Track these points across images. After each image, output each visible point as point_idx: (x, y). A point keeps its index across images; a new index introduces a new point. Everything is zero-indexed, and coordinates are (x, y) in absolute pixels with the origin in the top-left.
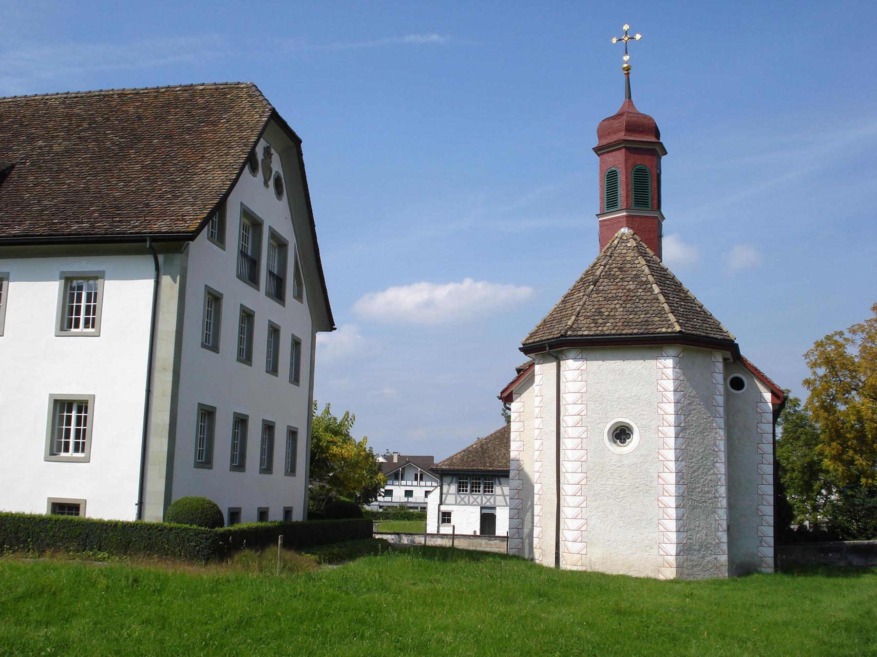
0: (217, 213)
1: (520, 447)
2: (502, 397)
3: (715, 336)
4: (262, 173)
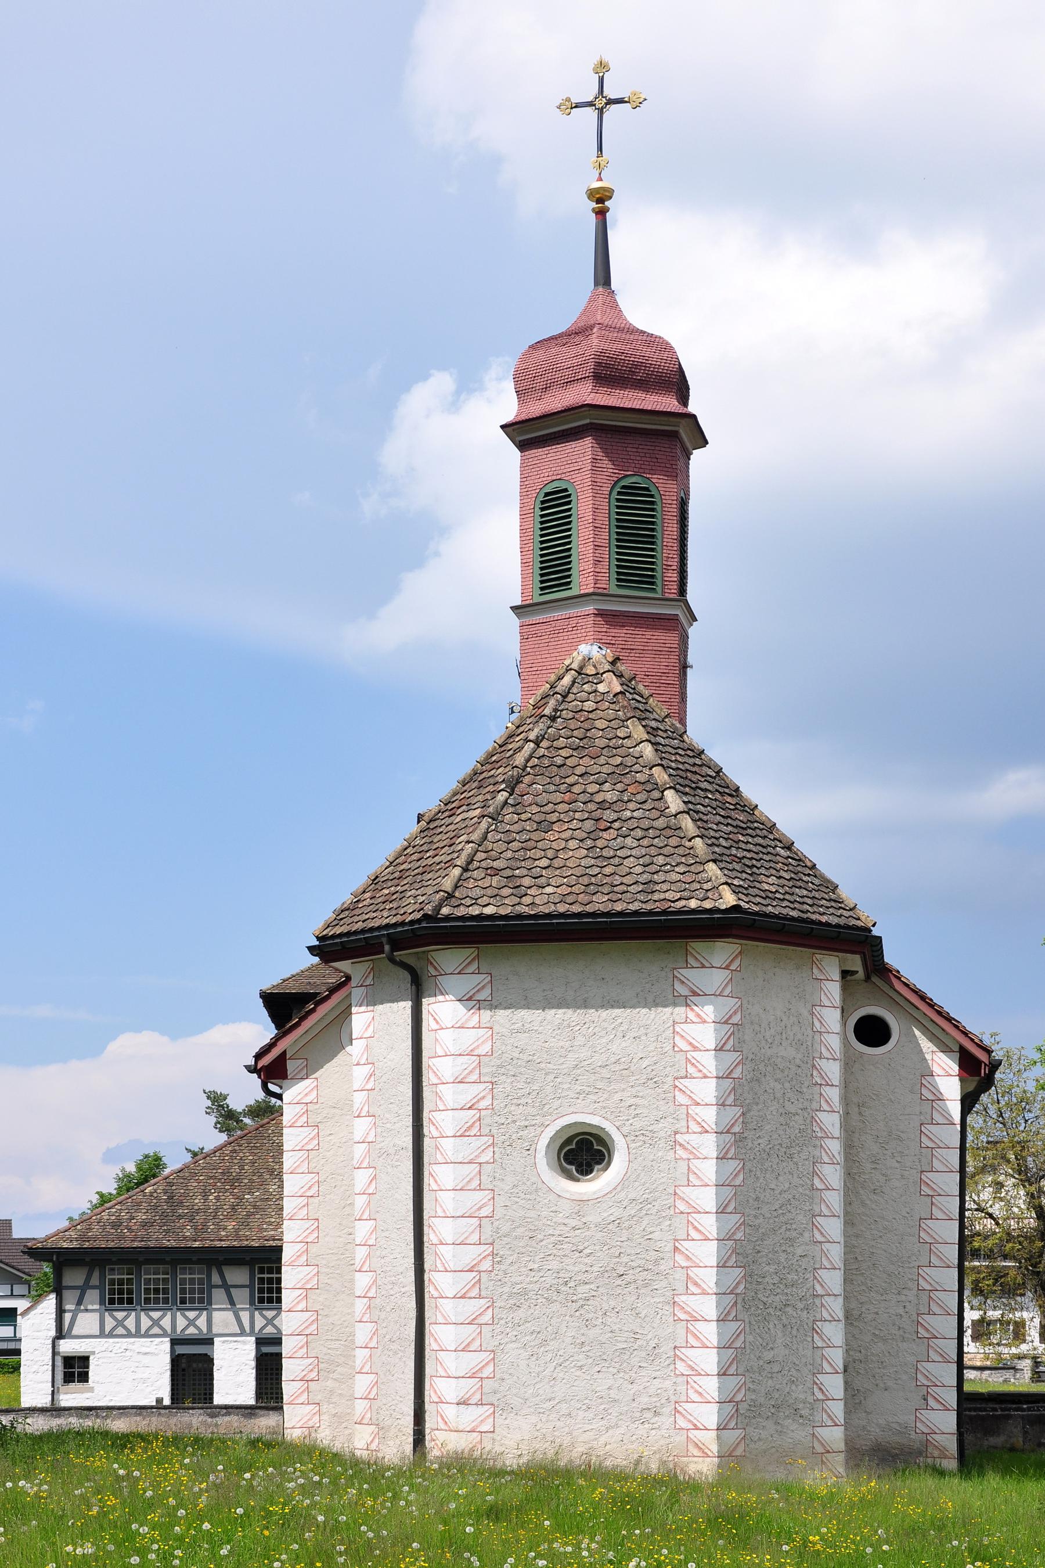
1: (310, 1188)
2: (259, 1066)
3: (824, 919)
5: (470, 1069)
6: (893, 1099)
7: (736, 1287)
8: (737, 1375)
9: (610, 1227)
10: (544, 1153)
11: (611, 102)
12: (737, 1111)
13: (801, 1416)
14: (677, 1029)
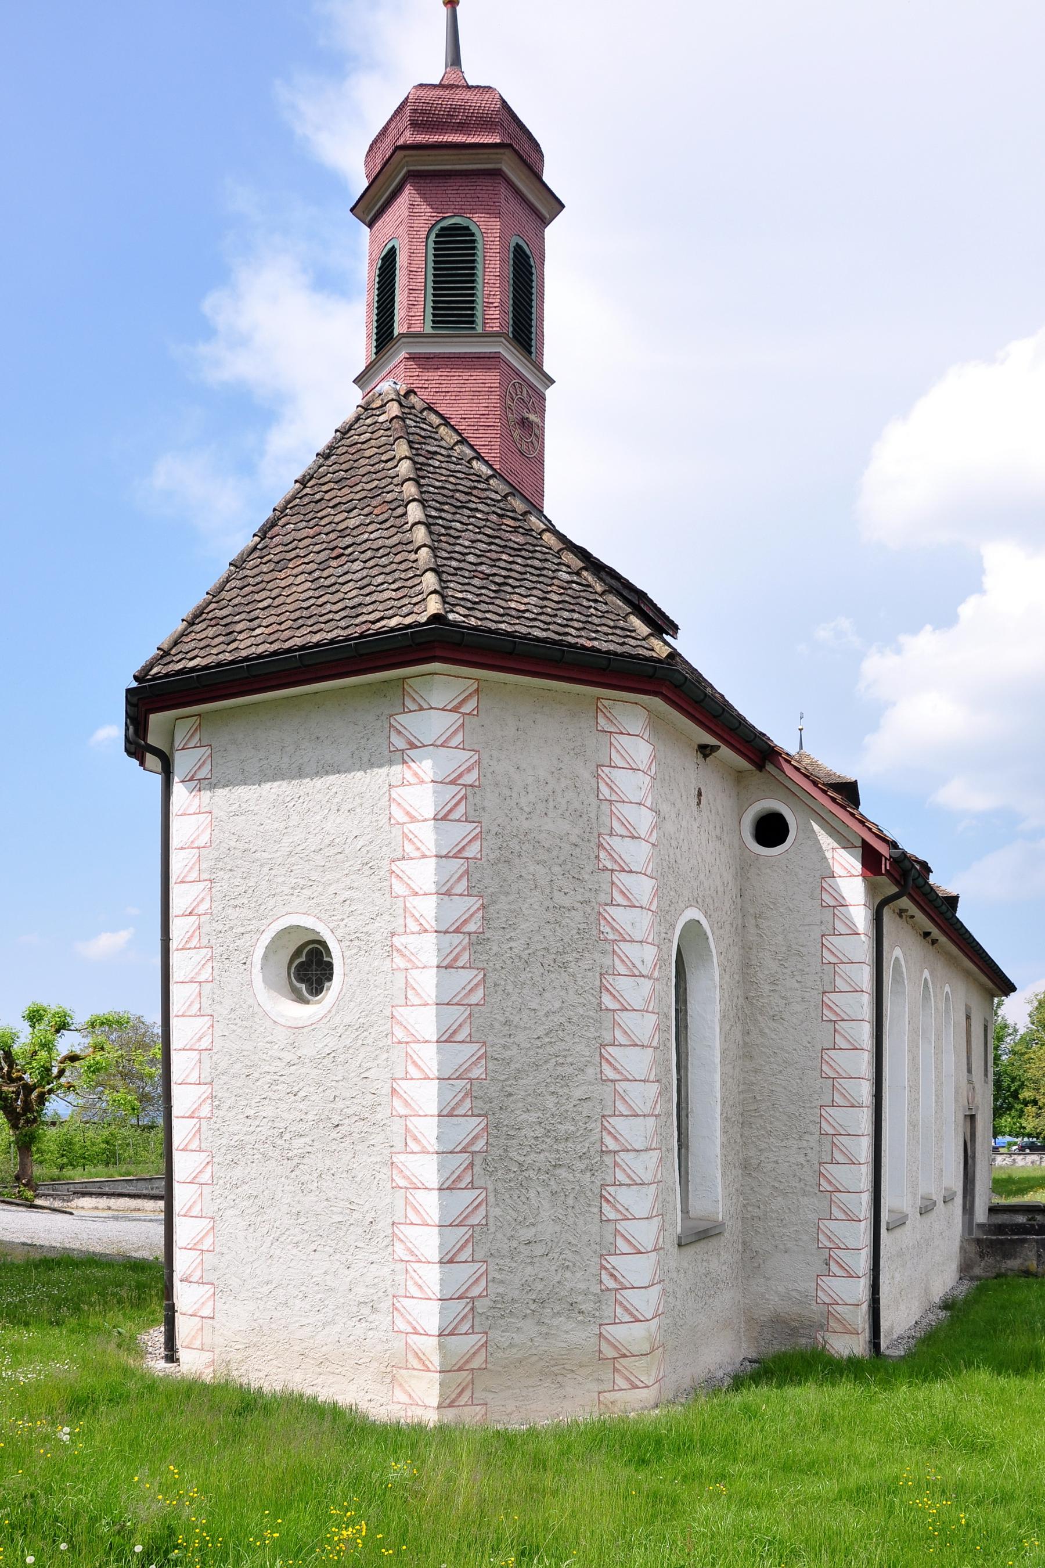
5: (190, 865)
6: (791, 907)
8: (473, 1261)
9: (326, 1061)
10: (259, 966)
12: (474, 903)
13: (581, 1312)
14: (394, 795)
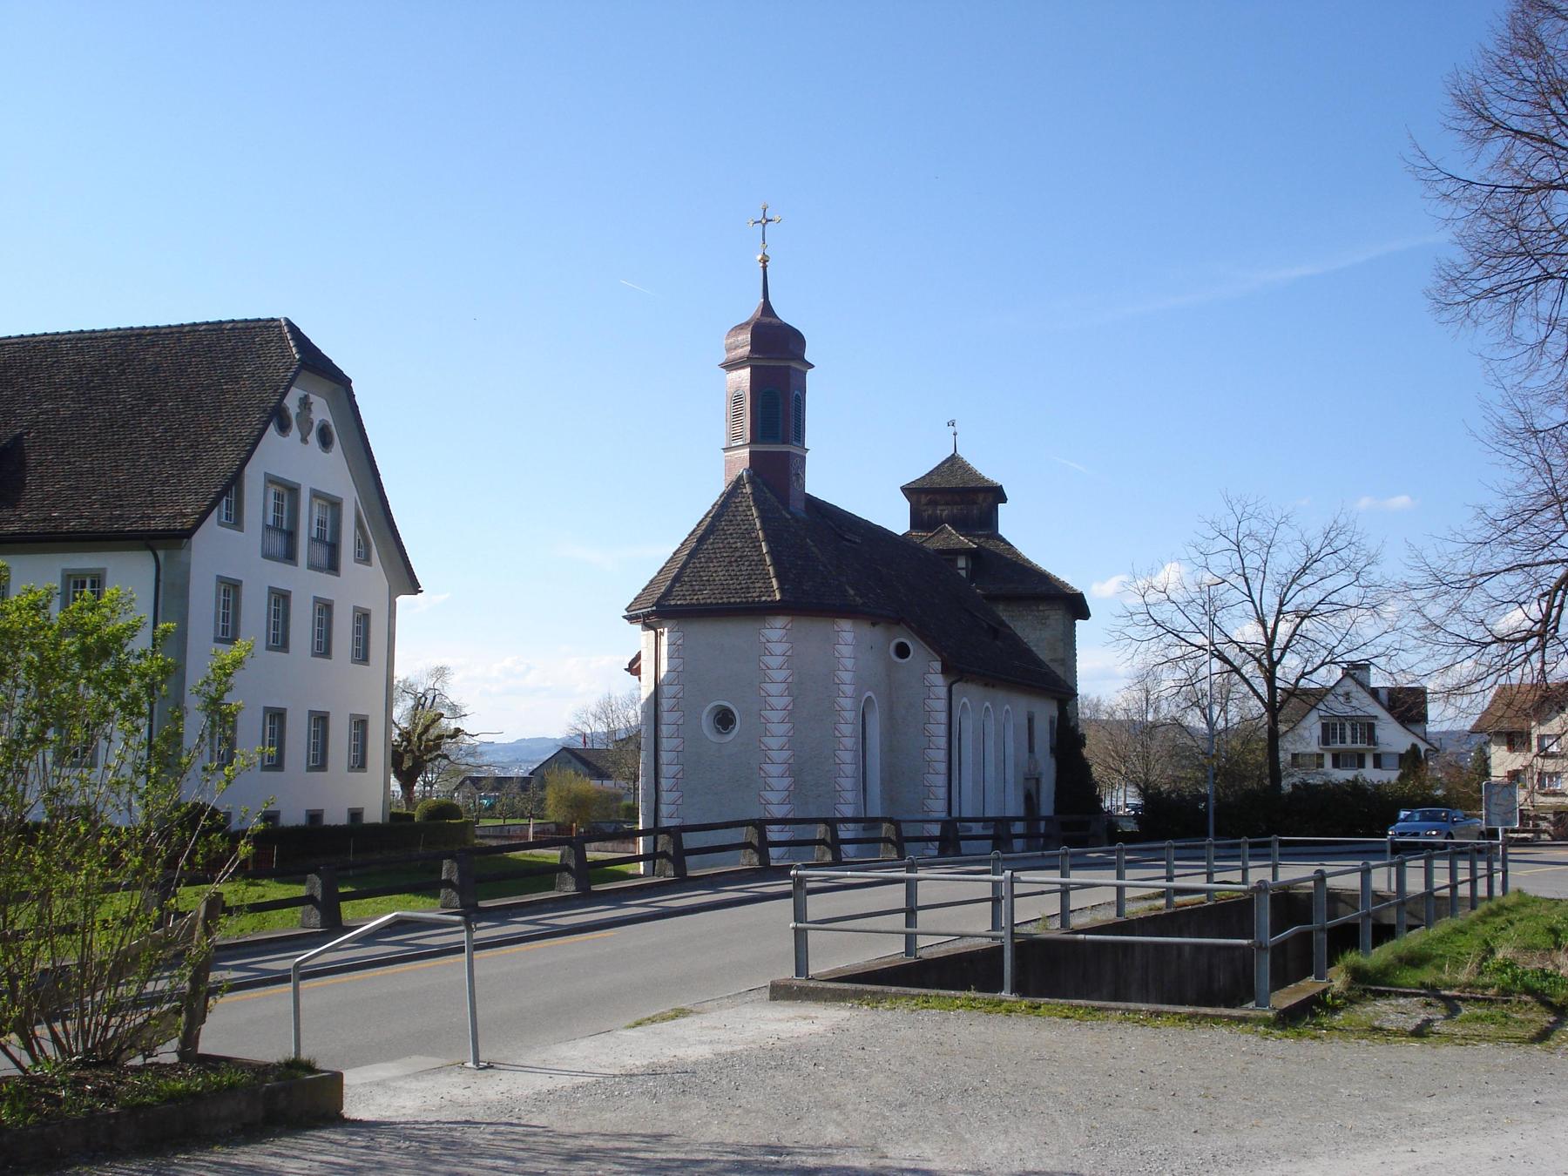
0: (234, 488)
4: (297, 428)
7: (789, 787)
11: (768, 221)
12: (790, 699)
